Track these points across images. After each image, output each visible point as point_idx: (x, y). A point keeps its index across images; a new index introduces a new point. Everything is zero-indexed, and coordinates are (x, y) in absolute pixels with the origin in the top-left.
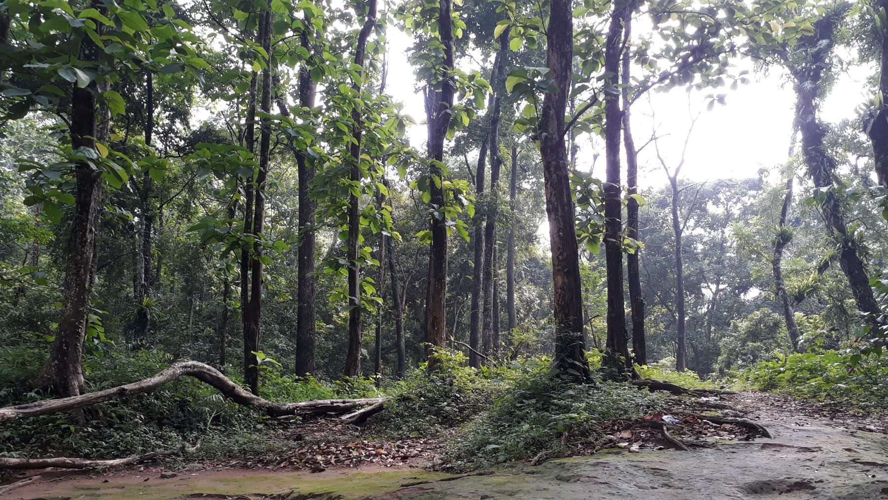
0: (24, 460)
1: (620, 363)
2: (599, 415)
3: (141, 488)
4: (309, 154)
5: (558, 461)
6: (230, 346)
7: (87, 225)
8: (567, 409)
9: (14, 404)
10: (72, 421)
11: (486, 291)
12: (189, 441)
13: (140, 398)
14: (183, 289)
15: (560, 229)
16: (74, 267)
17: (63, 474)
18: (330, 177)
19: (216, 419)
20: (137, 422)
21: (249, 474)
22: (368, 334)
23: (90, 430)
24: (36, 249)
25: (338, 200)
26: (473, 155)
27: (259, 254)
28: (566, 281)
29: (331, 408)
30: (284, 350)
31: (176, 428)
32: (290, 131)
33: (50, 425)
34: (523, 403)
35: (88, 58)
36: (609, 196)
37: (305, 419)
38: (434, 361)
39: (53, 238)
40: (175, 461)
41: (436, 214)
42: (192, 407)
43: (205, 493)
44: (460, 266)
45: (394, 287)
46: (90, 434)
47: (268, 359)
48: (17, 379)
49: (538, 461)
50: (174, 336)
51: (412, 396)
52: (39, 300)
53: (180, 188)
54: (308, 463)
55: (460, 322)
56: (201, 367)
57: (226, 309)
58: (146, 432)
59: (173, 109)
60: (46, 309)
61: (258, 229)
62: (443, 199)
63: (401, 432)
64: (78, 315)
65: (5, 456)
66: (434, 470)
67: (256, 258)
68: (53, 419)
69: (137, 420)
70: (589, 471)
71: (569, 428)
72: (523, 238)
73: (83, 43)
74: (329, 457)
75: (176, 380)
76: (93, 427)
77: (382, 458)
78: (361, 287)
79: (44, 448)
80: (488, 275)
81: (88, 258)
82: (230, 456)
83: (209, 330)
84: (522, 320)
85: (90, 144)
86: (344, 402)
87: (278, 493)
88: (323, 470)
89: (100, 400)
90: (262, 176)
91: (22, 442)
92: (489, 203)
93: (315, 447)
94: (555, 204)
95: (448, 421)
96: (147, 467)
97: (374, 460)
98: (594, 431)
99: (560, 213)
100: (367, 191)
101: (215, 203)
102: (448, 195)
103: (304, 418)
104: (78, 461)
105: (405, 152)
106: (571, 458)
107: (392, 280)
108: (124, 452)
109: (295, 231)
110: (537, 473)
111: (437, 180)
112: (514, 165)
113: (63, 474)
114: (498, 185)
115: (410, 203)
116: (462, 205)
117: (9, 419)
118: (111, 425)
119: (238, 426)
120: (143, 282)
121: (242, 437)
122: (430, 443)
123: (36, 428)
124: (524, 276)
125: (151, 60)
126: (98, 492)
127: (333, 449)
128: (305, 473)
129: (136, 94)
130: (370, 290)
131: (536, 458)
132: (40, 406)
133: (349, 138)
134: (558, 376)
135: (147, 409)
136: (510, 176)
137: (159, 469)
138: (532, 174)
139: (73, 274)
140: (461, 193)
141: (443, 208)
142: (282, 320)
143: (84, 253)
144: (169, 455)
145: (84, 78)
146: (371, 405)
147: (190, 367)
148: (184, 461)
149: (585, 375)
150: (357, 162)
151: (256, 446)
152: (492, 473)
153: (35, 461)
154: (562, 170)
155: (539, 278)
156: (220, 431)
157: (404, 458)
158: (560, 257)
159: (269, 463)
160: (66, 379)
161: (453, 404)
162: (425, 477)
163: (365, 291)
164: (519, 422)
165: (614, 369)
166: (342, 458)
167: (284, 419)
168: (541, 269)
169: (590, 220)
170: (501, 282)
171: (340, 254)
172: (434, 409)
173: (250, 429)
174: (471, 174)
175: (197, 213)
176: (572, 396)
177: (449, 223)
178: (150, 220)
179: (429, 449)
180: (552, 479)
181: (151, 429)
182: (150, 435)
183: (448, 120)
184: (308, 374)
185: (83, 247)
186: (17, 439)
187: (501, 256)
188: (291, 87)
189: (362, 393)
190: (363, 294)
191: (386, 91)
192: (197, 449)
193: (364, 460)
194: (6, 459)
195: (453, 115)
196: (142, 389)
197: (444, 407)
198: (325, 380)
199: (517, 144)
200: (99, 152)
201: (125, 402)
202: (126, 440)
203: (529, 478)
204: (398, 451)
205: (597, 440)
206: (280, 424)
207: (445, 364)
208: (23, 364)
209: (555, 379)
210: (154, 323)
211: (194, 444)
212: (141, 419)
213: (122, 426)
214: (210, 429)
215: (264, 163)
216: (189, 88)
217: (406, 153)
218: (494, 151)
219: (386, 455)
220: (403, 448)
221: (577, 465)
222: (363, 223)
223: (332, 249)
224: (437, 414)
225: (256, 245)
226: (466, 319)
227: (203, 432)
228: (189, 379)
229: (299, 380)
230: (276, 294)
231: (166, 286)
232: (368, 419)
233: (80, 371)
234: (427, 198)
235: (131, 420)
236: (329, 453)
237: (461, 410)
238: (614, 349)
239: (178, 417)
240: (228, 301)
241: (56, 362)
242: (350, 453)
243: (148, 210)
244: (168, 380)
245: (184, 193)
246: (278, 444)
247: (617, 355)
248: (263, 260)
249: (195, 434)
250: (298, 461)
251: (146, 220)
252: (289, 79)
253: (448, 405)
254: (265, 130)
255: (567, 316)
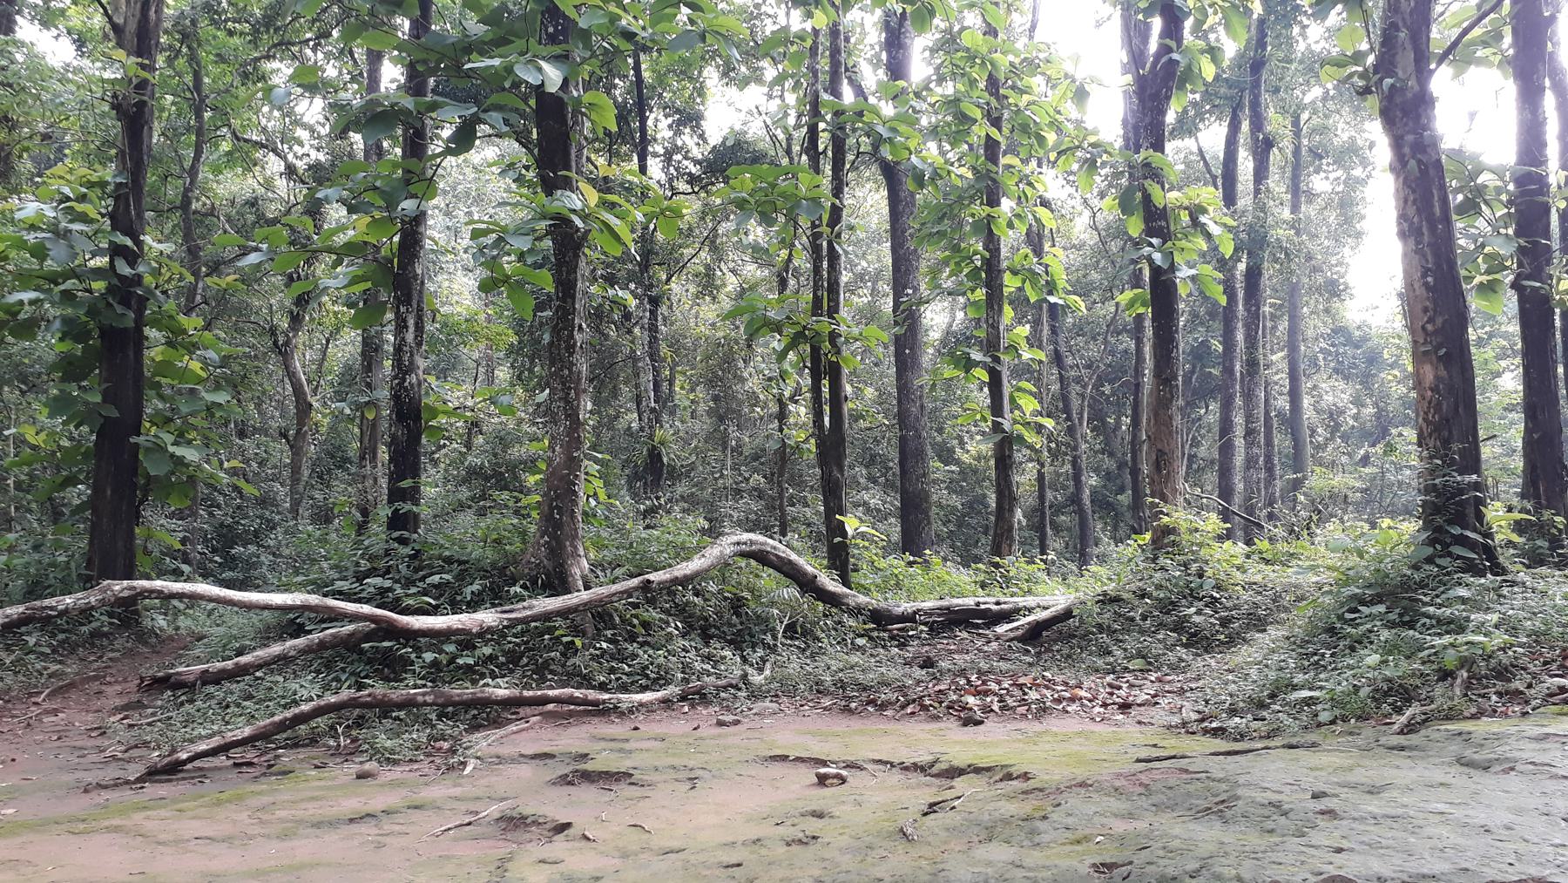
0: (516, 692)
1: (1554, 531)
2: (1529, 636)
3: (691, 741)
4: (915, 168)
5: (1454, 727)
6: (793, 505)
7: (573, 319)
8: (1457, 626)
9: (494, 605)
10: (577, 630)
11: (1249, 396)
12: (752, 665)
13: (672, 593)
14: (710, 412)
15: (1429, 270)
16: (560, 387)
17: (571, 714)
18: (950, 205)
19: (791, 629)
20: (670, 633)
21: (855, 723)
22: (1024, 478)
23: (604, 645)
24: (490, 359)
25: (963, 245)
26: (1213, 136)
27: (838, 352)
28: (1443, 373)
29: (977, 612)
30: (879, 510)
31: (730, 642)
32: (880, 129)
33: (546, 637)
34: (1359, 611)
35: (553, 40)
36: (1523, 194)
37: (935, 629)
38: (1163, 532)
39: (514, 339)
40: (735, 697)
41: (1157, 257)
42: (752, 608)
43: (793, 754)
44: (1192, 351)
45: (1065, 398)
46: (604, 651)
47: (863, 529)
48: (493, 565)
49: (1407, 726)
50: (702, 489)
51: (1125, 596)
52: (503, 440)
53: (697, 245)
54: (952, 708)
55: (1195, 456)
56: (762, 544)
57: (784, 443)
58: (683, 650)
59: (678, 111)
60: (517, 452)
61: (833, 310)
62: (1168, 227)
63: (1112, 659)
64: (573, 463)
65: (488, 685)
66: (1187, 732)
67: (834, 359)
68: (549, 628)
69: (670, 629)
70: (1530, 751)
71: (1465, 662)
72: (1319, 290)
73: (543, 16)
74: (989, 699)
75: (724, 566)
76: (609, 641)
77: (1082, 705)
78: (1012, 400)
79: (541, 672)
80: (1252, 365)
81: (580, 372)
82: (819, 692)
83: (758, 479)
84: (1319, 447)
85: (567, 184)
86: (998, 603)
87: (912, 761)
88: (979, 723)
89: (615, 599)
90: (836, 213)
91: (510, 663)
92: (1251, 226)
93: (962, 682)
94: (1415, 220)
95: (1199, 641)
96: (693, 706)
97: (1069, 709)
98: (1523, 669)
99: (1426, 239)
100: (1016, 222)
101: (751, 267)
102: (1177, 218)
103: (931, 629)
104: (592, 695)
105: (1090, 145)
106: (1478, 722)
107: (1061, 382)
108: (655, 681)
109: (887, 305)
110: (1411, 748)
111: (1155, 191)
112: (1297, 152)
113: (571, 714)
114: (1268, 190)
115: (1091, 238)
116: (1208, 236)
117: (490, 630)
118: (632, 638)
119: (826, 640)
120: (653, 405)
121: (834, 661)
122: (1169, 682)
123: (526, 643)
124: (1322, 363)
125: (650, 31)
126: (627, 746)
127: (993, 686)
128: (950, 726)
129: (617, 92)
130: (1029, 405)
131: (1403, 719)
132: (530, 608)
133: (981, 130)
134: (1430, 560)
135: (682, 611)
136: (1289, 169)
137: (711, 710)
138: (1335, 163)
139: (560, 399)
140: (1204, 211)
141: (1169, 244)
142: (871, 460)
143: (572, 364)
144: (725, 688)
145: (553, 76)
146: (1045, 608)
147: (745, 543)
148: (748, 698)
149: (1487, 560)
150: (997, 173)
151: (860, 677)
152: (1314, 745)
153: (531, 693)
154: (1429, 150)
155: (1355, 366)
156: (798, 648)
157: (1125, 707)
158: (1429, 327)
159: (883, 707)
160: (562, 565)
161: (1208, 611)
162: (1173, 744)
163: (1019, 407)
164: (1353, 649)
165: (1539, 543)
166: (1010, 701)
167: (899, 629)
168: (1357, 347)
169: (1483, 246)
170: (1276, 378)
171: (966, 339)
172: (1169, 619)
173: (846, 645)
174: (1209, 171)
175: (724, 285)
176: (1464, 601)
177: (1184, 272)
178: (655, 302)
179: (1168, 692)
180: (1450, 764)
181: (693, 644)
182: (692, 654)
183: (1175, 74)
184: (927, 552)
185: (571, 354)
186: (502, 659)
187: (1274, 328)
188: (868, 48)
189: (1025, 586)
190: (1017, 412)
191: (1039, 35)
192: (766, 679)
193: (1050, 708)
194: (491, 690)
195: (1183, 63)
196: (676, 581)
197: (1190, 616)
198: (953, 561)
199: (1301, 107)
200: (579, 199)
201: (652, 602)
202: (656, 662)
203: (1398, 759)
204: (1111, 694)
205: (1530, 686)
206: (892, 638)
207: (1186, 537)
208: (498, 541)
209: (1427, 567)
210: (672, 469)
211: (761, 670)
212: (677, 628)
213: (649, 639)
214: (783, 645)
215: (837, 191)
216: (700, 73)
217: (1093, 145)
218: (1257, 123)
219: (1090, 701)
220: (1119, 688)
221: (1498, 737)
222: (1010, 283)
223: (948, 333)
224: (1178, 627)
225: (833, 336)
226: (1207, 449)
227: (772, 649)
228: (742, 563)
229: (915, 562)
230: (862, 417)
231: (685, 408)
232: (1045, 634)
233: (582, 553)
234: (1135, 227)
235: (663, 629)
236: (986, 693)
237: (1225, 622)
238: (1539, 503)
239: (731, 625)
240: (786, 431)
241: (546, 538)
242: (1025, 694)
243: (651, 286)
244: (713, 567)
245: (703, 254)
246: (893, 673)
247: (1547, 514)
248: (845, 360)
249: (760, 652)
250: (936, 705)
251: (650, 302)
252: (864, 33)
253: (1199, 612)
254: (838, 133)
255: (1446, 443)
